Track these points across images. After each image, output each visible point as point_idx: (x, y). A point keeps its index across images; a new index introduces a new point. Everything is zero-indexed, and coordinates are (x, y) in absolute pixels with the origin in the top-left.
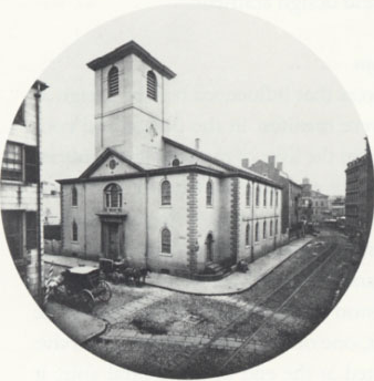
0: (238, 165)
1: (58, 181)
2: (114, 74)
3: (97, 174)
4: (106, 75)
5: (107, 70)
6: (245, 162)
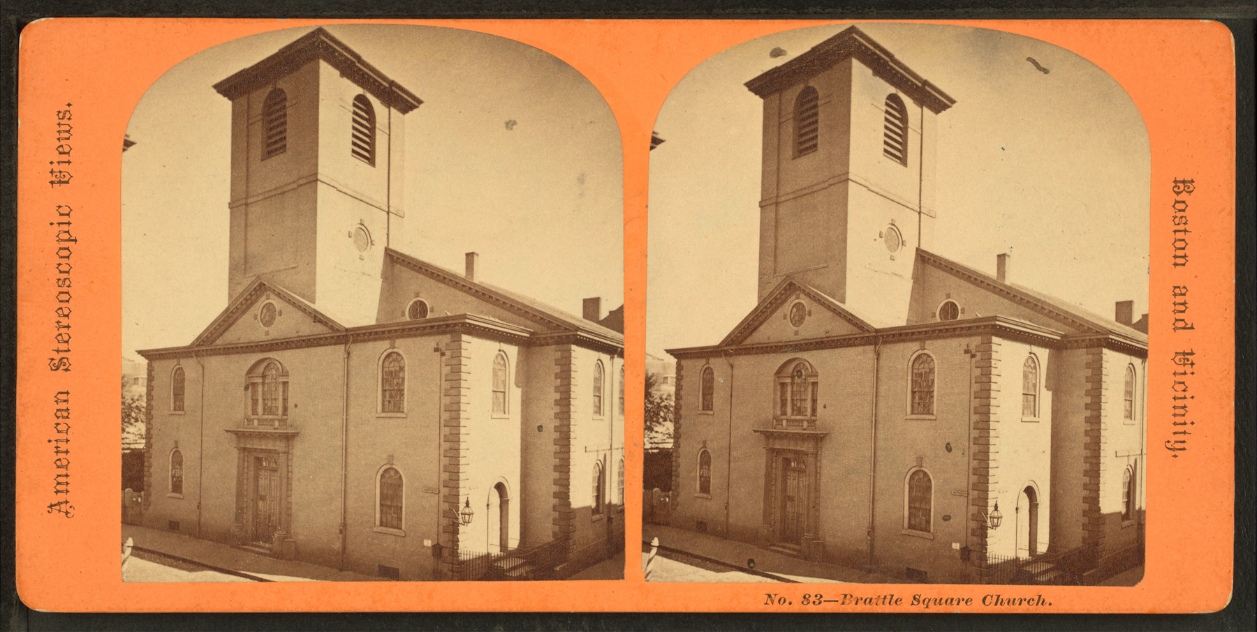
0: (572, 311)
2: (276, 101)
3: (232, 336)
4: (258, 108)
5: (792, 95)
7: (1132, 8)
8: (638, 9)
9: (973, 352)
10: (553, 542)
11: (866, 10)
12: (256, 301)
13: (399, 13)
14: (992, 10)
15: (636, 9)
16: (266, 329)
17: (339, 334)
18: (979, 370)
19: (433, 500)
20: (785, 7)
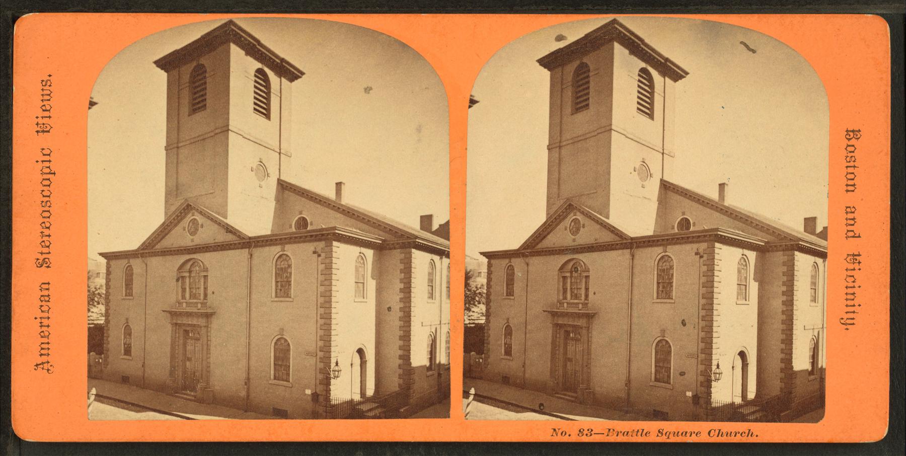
1: (102, 254)
2: (199, 73)
3: (168, 242)
4: (186, 78)
5: (571, 68)
6: (426, 221)
7: (816, 6)
8: (460, 7)
9: (702, 254)
10: (398, 391)
11: (624, 7)
12: (184, 217)
13: (287, 10)
14: (715, 7)
15: (458, 7)
16: (192, 237)
17: (244, 241)
18: (706, 267)
19: (312, 361)
20: (566, 5)
